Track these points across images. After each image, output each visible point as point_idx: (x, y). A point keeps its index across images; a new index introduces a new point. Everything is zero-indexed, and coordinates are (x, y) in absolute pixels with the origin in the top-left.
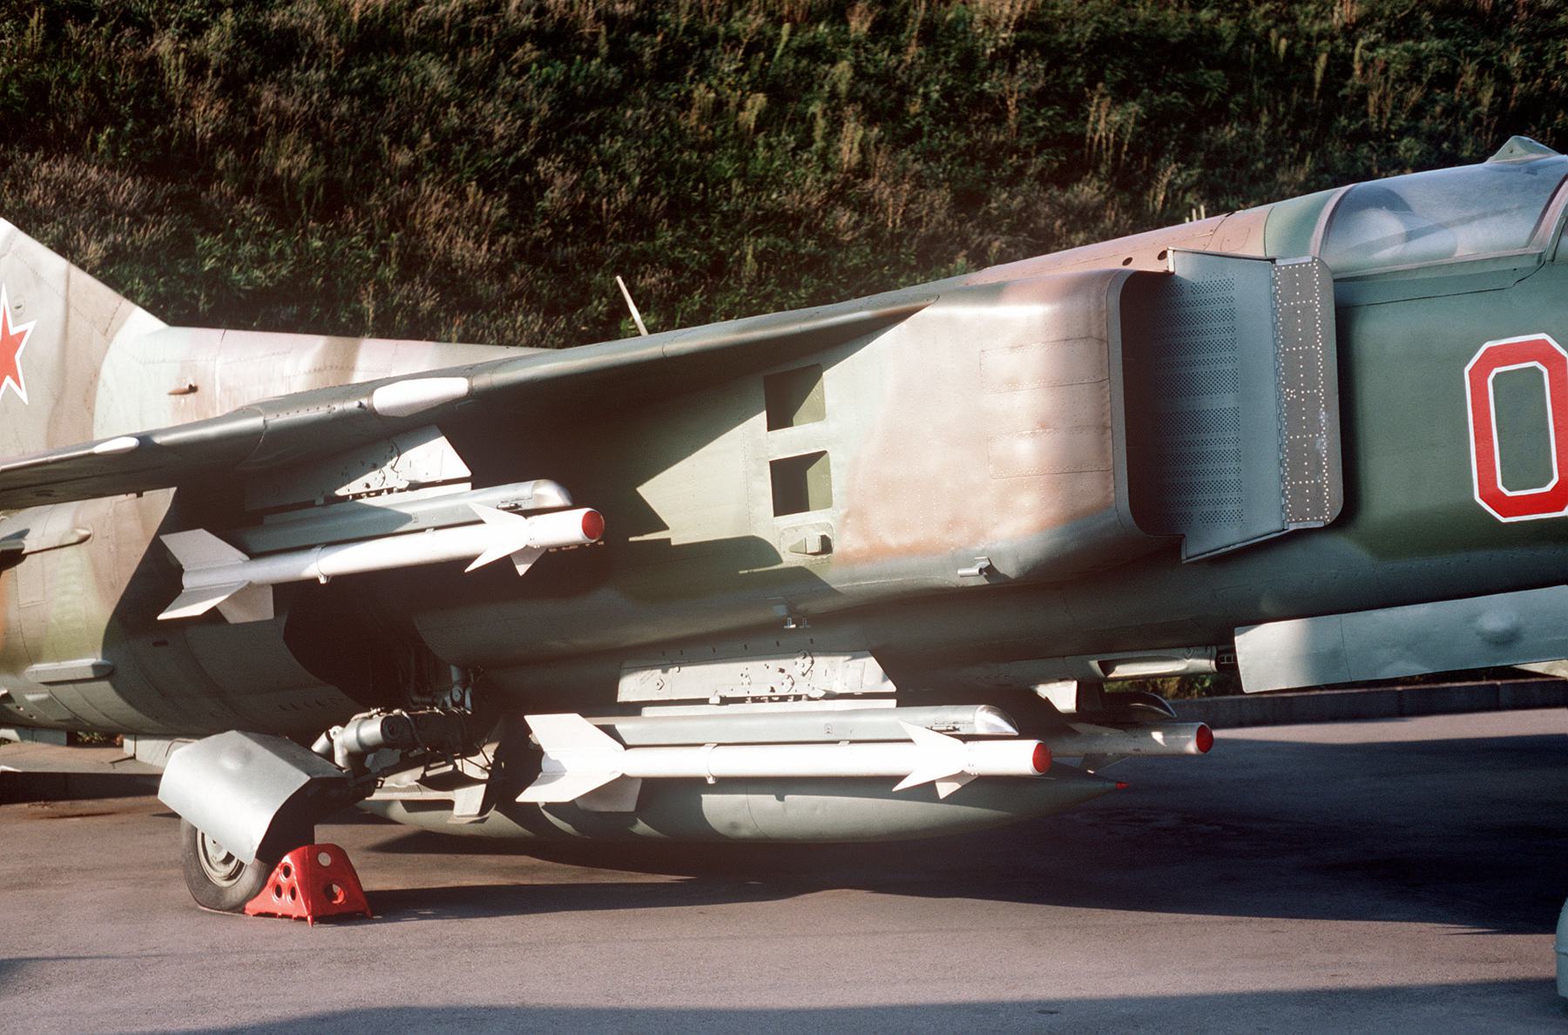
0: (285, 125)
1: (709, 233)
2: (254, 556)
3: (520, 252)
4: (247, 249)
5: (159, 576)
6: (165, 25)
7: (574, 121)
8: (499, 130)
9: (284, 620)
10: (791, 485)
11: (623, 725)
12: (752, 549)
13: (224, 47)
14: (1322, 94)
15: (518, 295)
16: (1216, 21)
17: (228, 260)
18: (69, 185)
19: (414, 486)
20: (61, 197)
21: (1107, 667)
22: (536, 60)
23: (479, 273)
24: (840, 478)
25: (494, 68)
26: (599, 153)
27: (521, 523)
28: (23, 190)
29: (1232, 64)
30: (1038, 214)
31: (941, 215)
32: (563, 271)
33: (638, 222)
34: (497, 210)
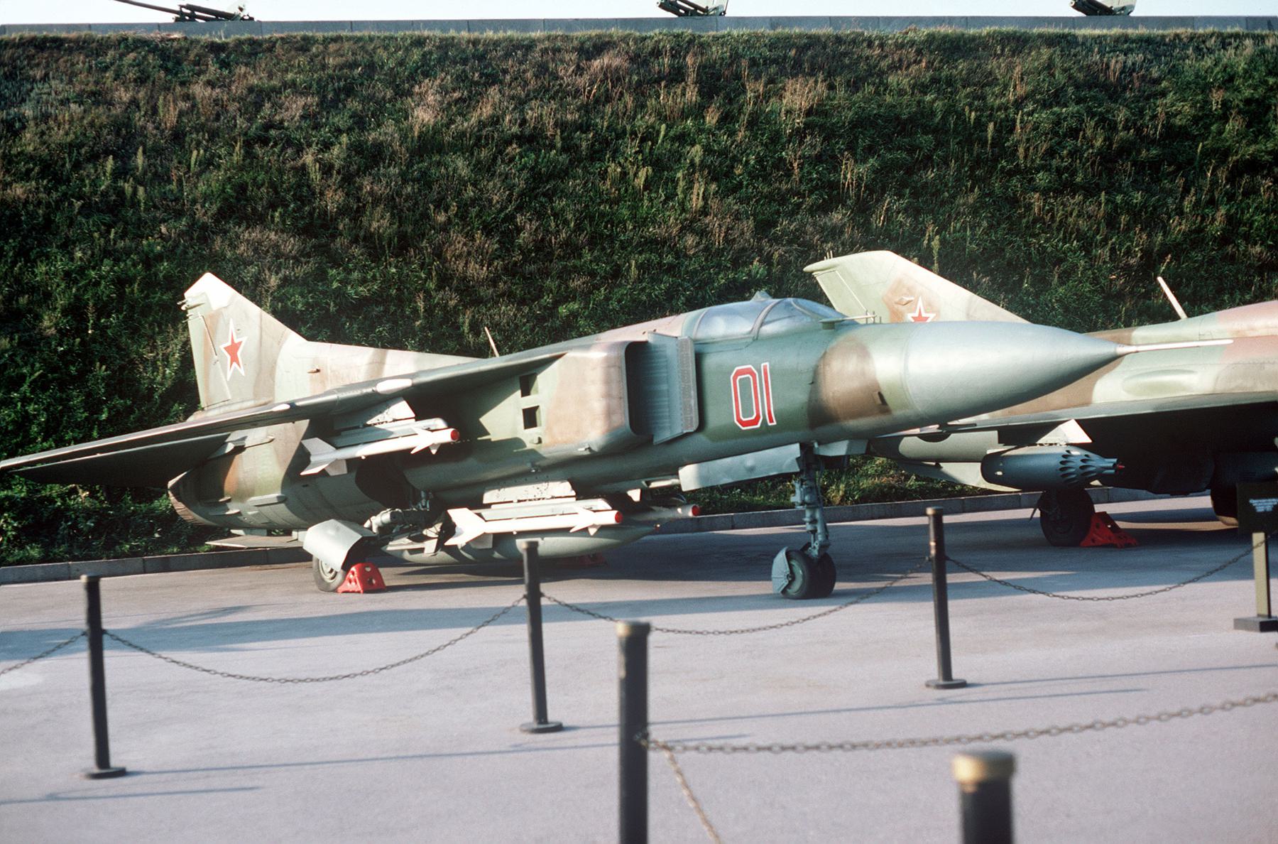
0: (377, 201)
1: (613, 253)
2: (337, 448)
3: (505, 268)
4: (356, 275)
5: (302, 457)
6: (309, 145)
7: (541, 186)
8: (496, 198)
9: (354, 474)
10: (530, 417)
11: (484, 512)
12: (517, 442)
13: (342, 156)
14: (993, 145)
15: (503, 295)
16: (934, 101)
17: (344, 282)
18: (260, 243)
19: (395, 420)
20: (256, 250)
21: (648, 483)
22: (520, 153)
23: (481, 283)
24: (542, 416)
25: (495, 159)
26: (552, 209)
27: (432, 434)
28: (236, 247)
29: (939, 131)
30: (805, 233)
31: (748, 235)
32: (528, 279)
33: (572, 249)
34: (492, 245)
